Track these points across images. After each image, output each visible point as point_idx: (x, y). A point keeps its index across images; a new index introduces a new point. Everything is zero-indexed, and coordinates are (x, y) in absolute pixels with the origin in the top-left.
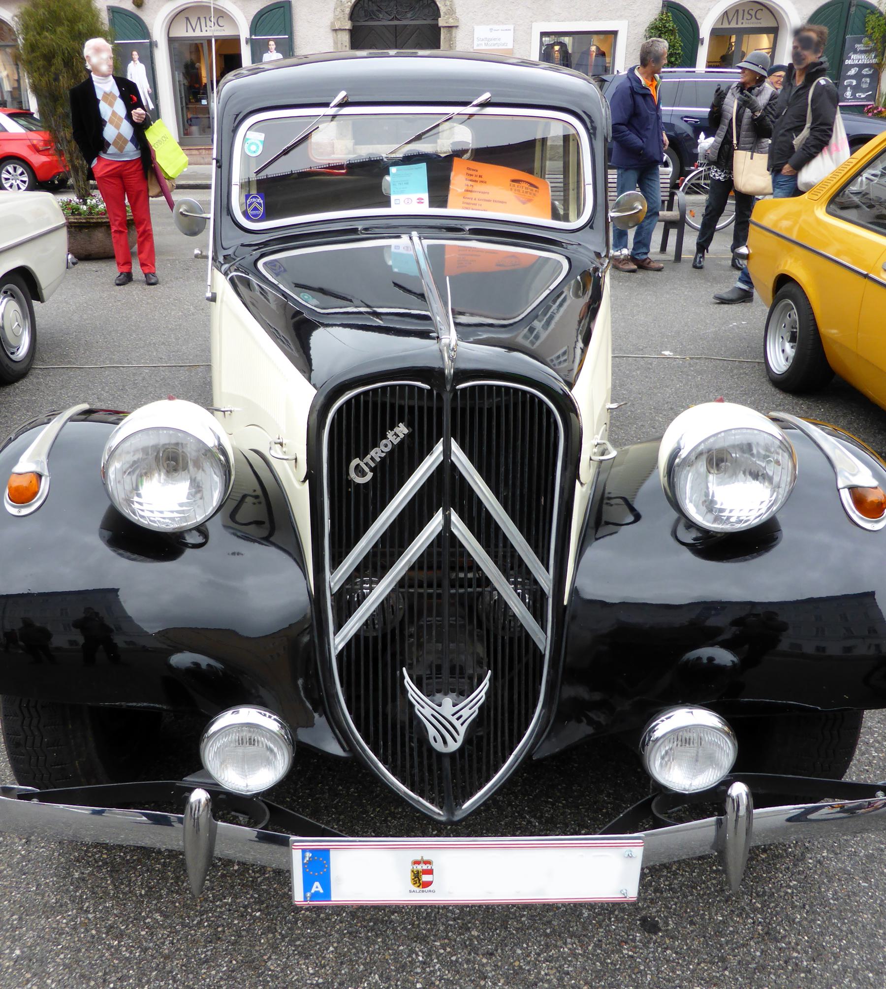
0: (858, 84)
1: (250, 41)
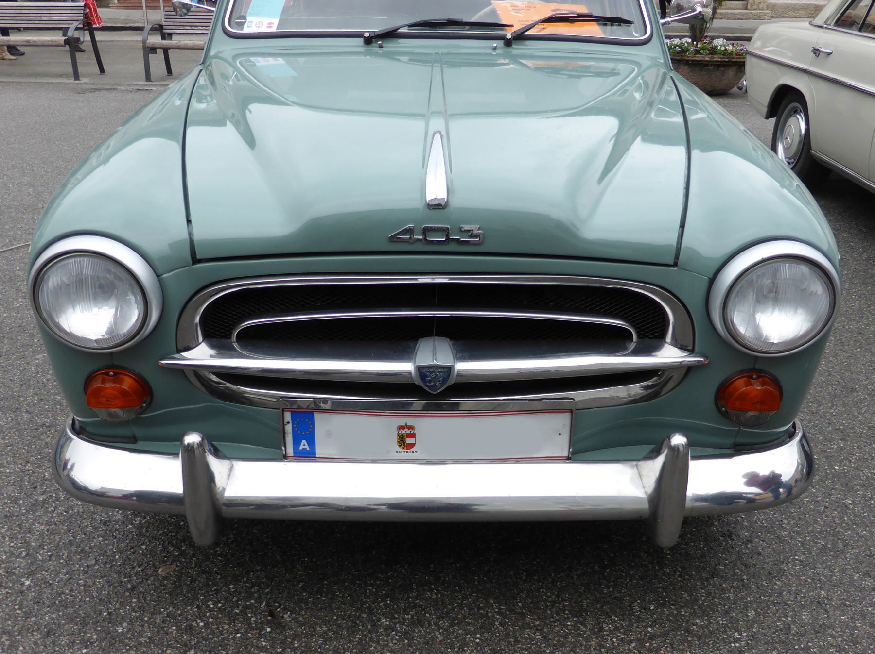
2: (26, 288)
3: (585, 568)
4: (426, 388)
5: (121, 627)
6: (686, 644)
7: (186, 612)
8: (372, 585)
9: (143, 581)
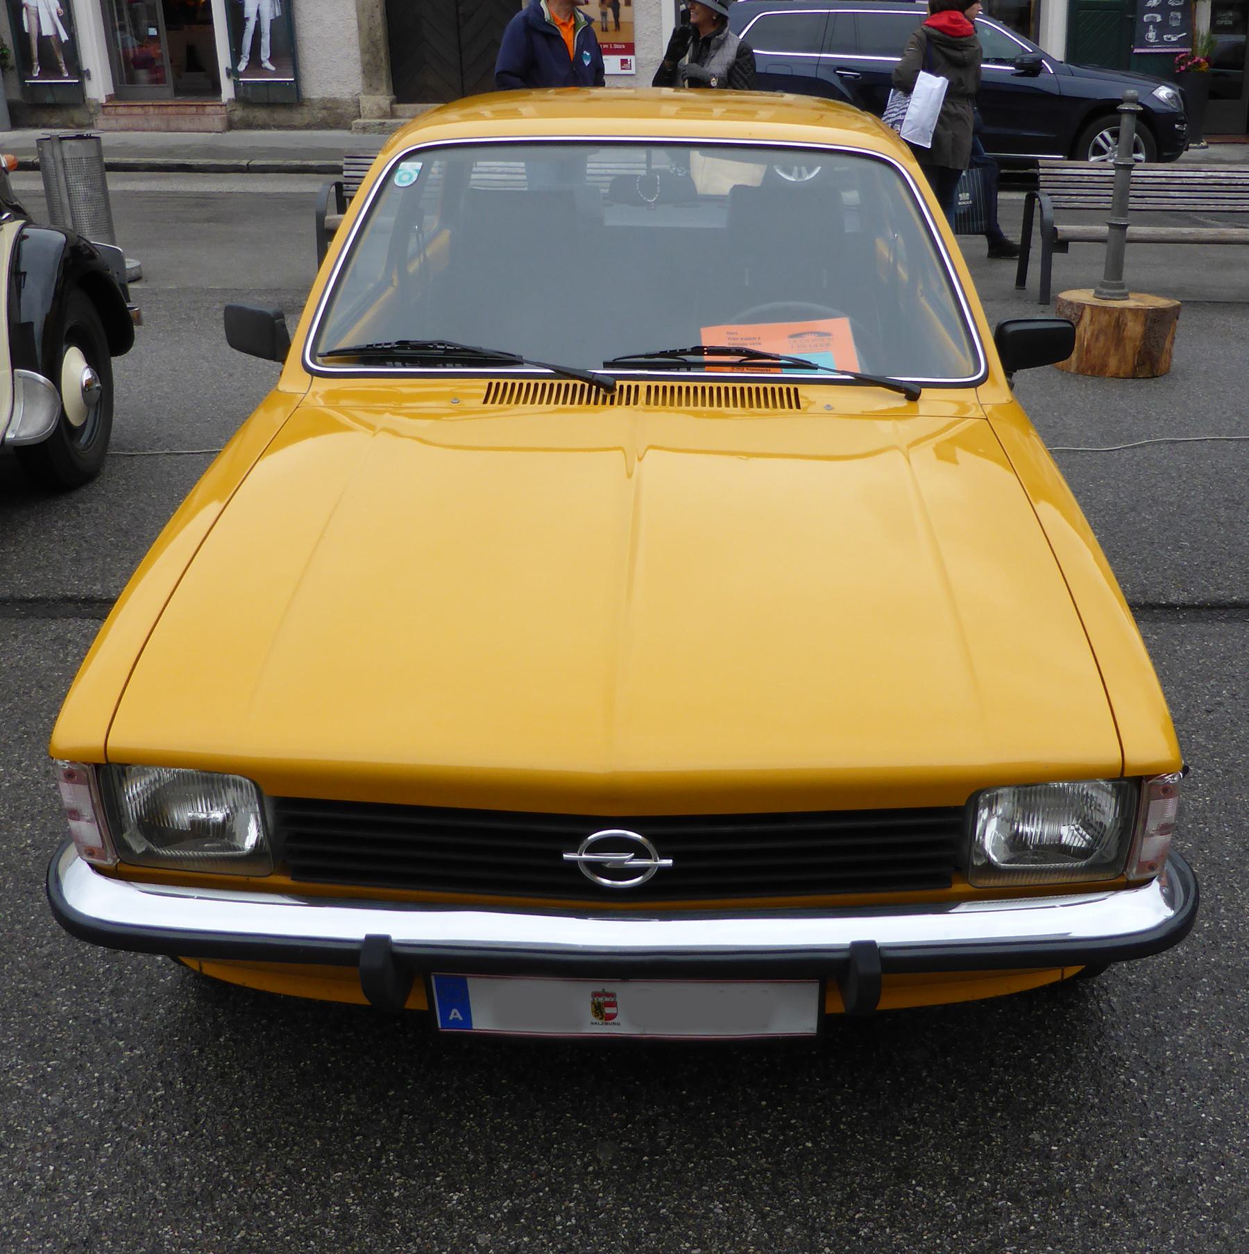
0: (1166, 18)
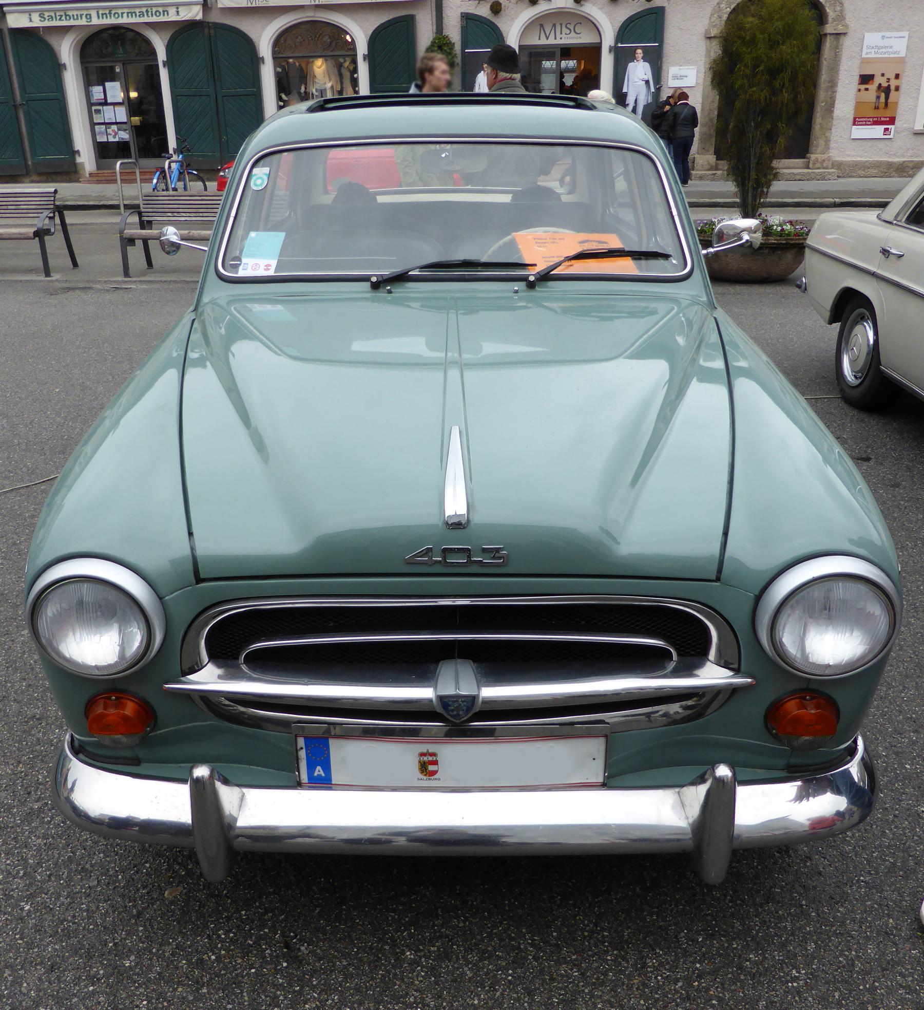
1: (615, 50)
2: (23, 611)
3: (626, 891)
4: (449, 717)
5: (129, 960)
6: (738, 984)
7: (195, 943)
8: (394, 911)
9: (148, 906)
